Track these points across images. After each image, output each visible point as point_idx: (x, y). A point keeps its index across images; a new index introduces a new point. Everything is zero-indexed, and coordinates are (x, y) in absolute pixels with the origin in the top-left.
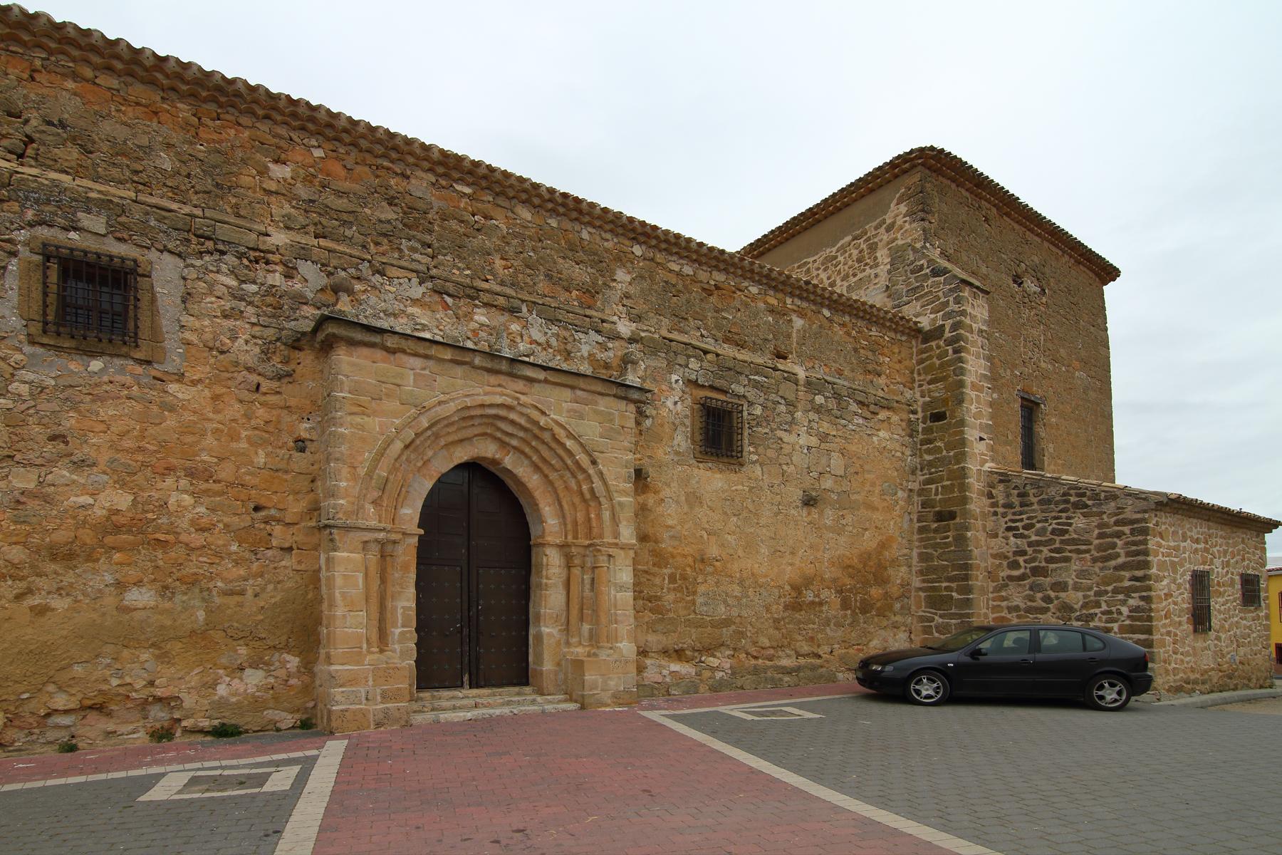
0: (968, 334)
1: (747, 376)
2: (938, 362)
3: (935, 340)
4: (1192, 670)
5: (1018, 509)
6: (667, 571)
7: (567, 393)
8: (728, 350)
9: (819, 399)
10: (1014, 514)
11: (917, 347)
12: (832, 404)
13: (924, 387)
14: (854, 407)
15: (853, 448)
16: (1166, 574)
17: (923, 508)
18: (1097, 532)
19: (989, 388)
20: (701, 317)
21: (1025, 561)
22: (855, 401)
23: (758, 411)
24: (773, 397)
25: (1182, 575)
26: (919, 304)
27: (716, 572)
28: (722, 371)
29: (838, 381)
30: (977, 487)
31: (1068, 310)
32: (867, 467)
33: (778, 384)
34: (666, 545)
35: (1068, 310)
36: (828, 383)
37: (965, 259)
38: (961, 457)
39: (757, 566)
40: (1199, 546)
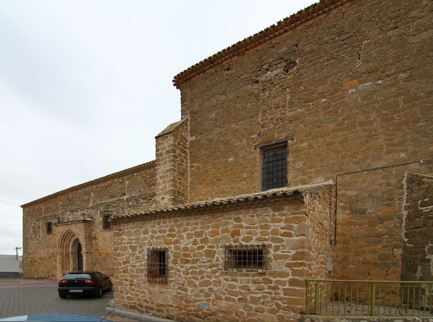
4: (145, 301)
6: (101, 257)
7: (74, 225)
9: (130, 203)
12: (135, 203)
14: (141, 201)
24: (118, 208)
27: (110, 257)
34: (101, 251)
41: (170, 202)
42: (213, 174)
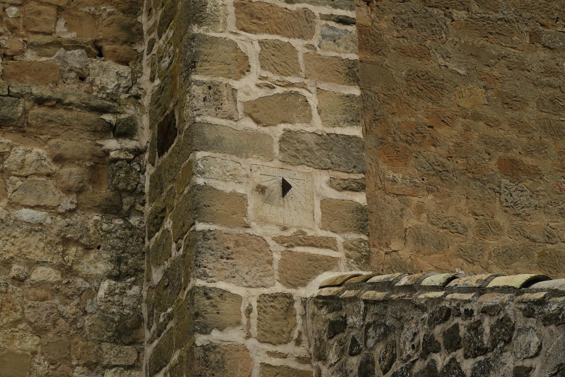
41: (339, 238)
42: (476, 117)
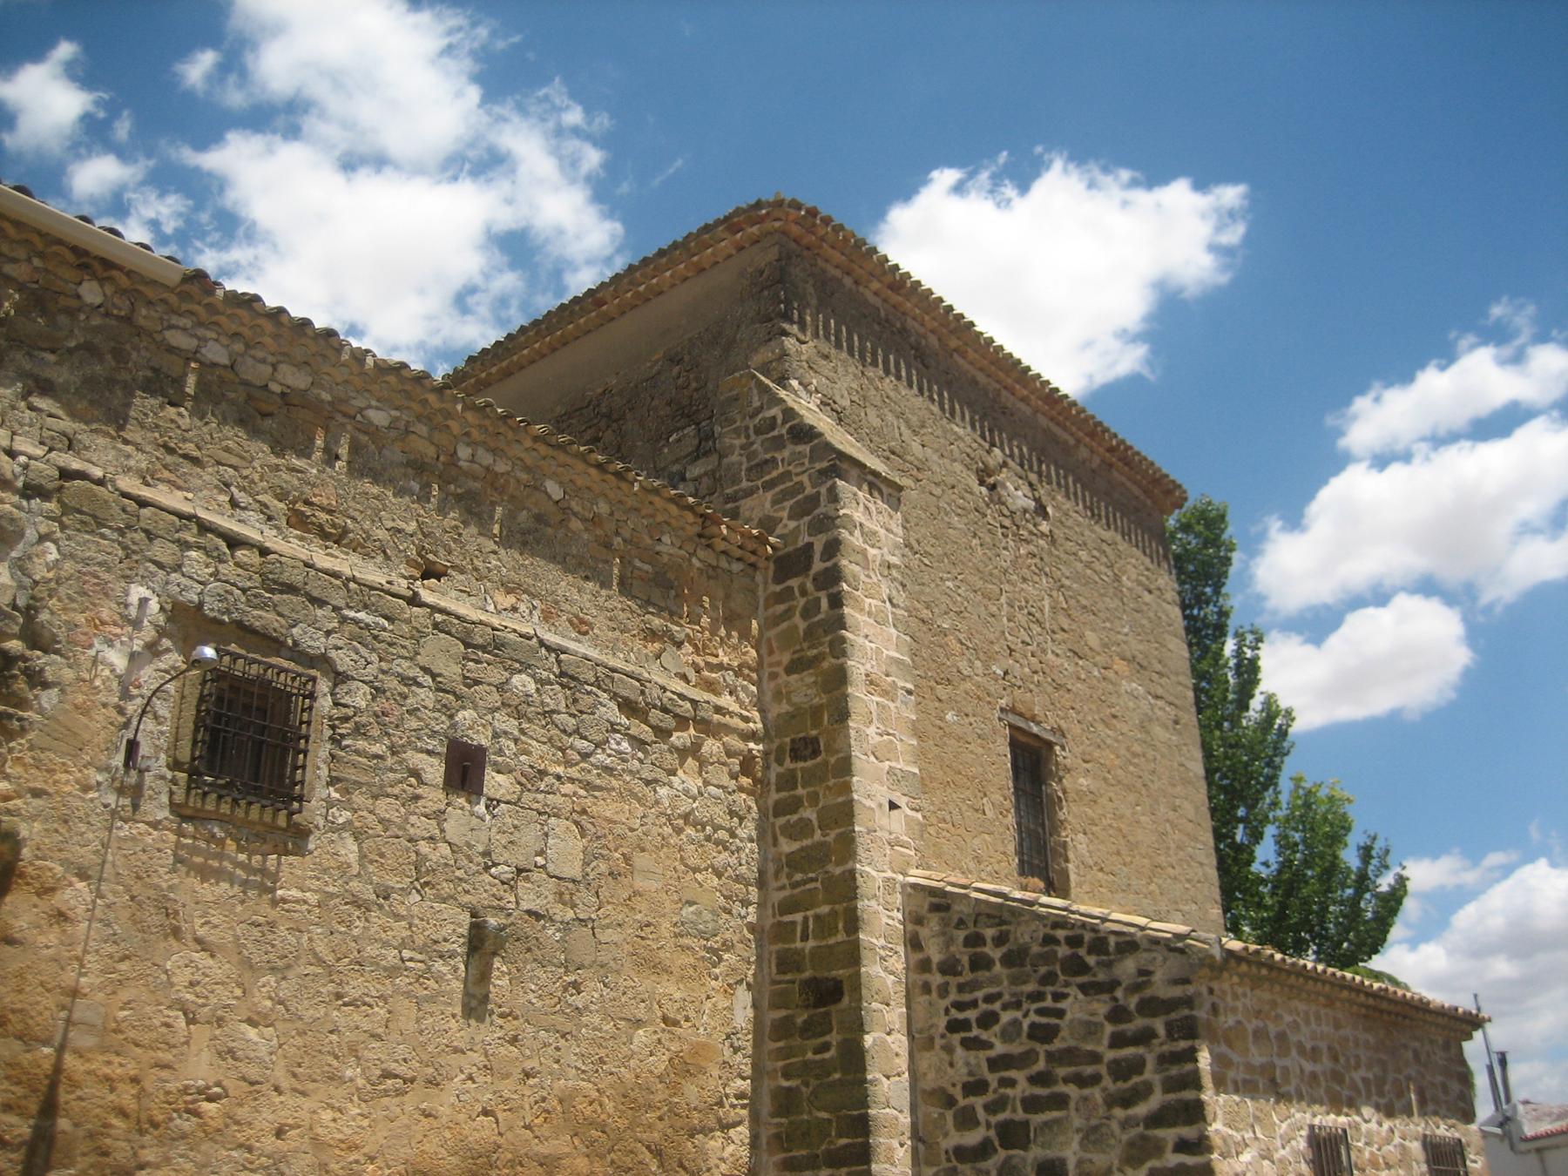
0: (857, 568)
1: (336, 609)
2: (802, 625)
3: (796, 575)
5: (967, 976)
8: (291, 546)
10: (961, 988)
11: (765, 589)
12: (555, 697)
13: (780, 681)
15: (606, 808)
16: (1249, 1135)
17: (780, 972)
18: (1109, 1029)
19: (909, 692)
20: (234, 461)
21: (987, 1108)
22: (615, 697)
23: (359, 697)
24: (403, 667)
25: (1287, 1141)
26: (769, 495)
28: (271, 591)
29: (572, 645)
30: (885, 920)
31: (1095, 553)
32: (640, 860)
33: (418, 636)
35: (1095, 553)
36: (549, 649)
37: (876, 422)
38: (847, 846)
39: (327, 1115)
40: (1318, 1068)
